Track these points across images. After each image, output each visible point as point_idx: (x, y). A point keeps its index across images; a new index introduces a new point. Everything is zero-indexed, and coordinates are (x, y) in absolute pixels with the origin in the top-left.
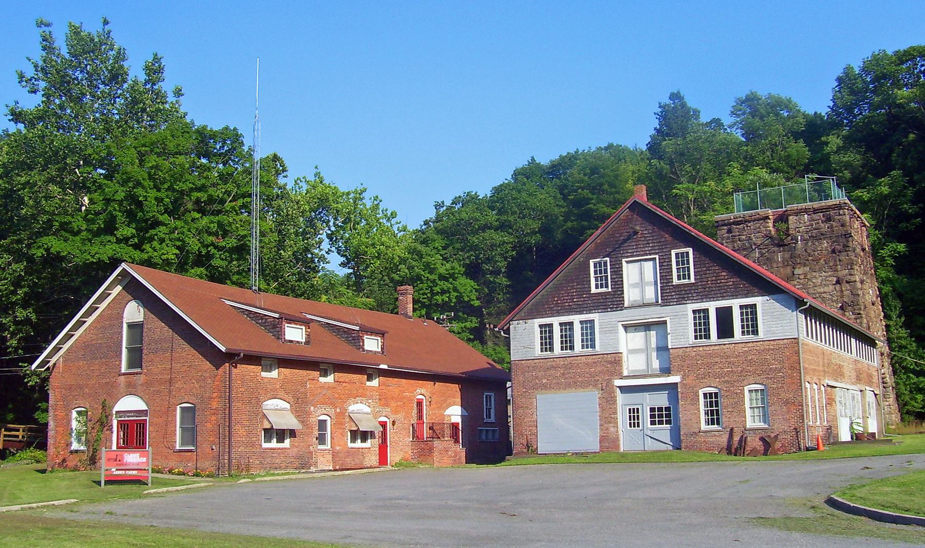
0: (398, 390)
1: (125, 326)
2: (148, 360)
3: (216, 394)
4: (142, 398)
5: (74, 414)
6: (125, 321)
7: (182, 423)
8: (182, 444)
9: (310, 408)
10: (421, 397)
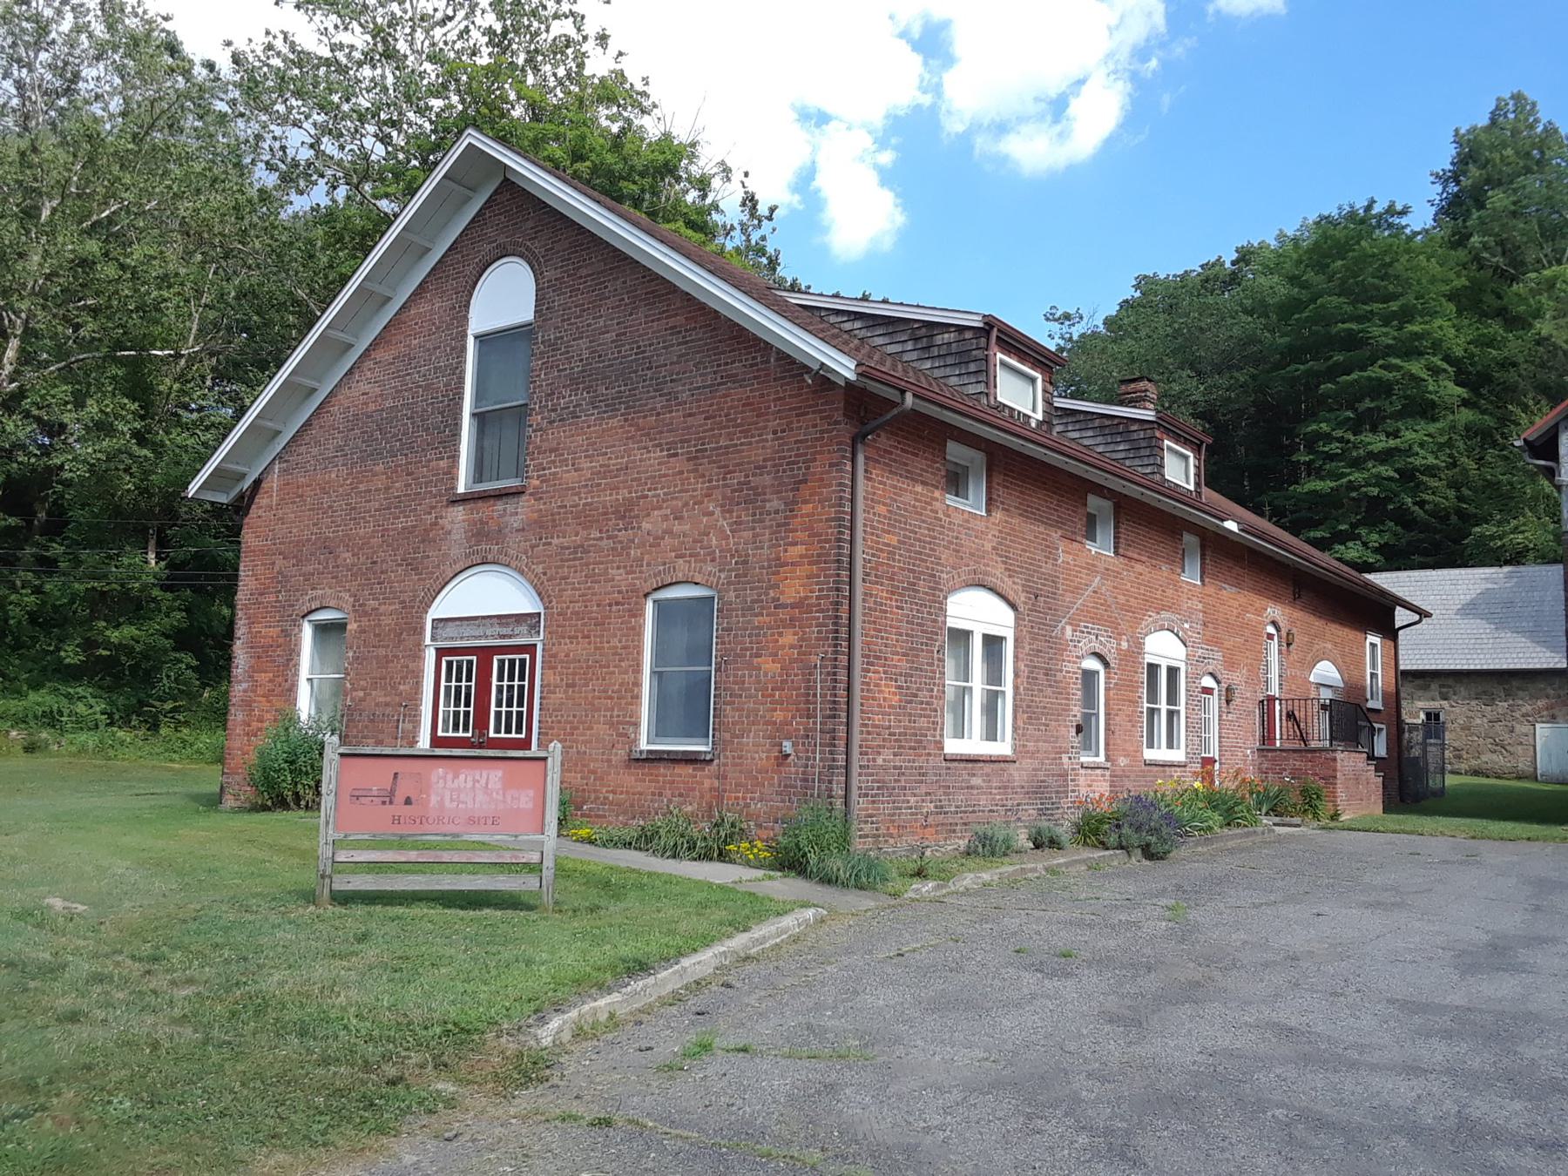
0: (1236, 604)
1: (471, 343)
2: (545, 445)
3: (800, 549)
4: (521, 572)
5: (307, 632)
6: (470, 332)
7: (659, 656)
8: (660, 731)
9: (1063, 628)
10: (1092, 664)
